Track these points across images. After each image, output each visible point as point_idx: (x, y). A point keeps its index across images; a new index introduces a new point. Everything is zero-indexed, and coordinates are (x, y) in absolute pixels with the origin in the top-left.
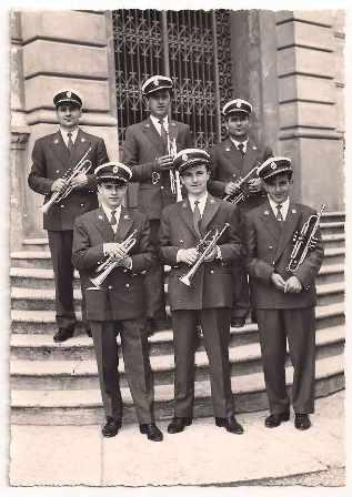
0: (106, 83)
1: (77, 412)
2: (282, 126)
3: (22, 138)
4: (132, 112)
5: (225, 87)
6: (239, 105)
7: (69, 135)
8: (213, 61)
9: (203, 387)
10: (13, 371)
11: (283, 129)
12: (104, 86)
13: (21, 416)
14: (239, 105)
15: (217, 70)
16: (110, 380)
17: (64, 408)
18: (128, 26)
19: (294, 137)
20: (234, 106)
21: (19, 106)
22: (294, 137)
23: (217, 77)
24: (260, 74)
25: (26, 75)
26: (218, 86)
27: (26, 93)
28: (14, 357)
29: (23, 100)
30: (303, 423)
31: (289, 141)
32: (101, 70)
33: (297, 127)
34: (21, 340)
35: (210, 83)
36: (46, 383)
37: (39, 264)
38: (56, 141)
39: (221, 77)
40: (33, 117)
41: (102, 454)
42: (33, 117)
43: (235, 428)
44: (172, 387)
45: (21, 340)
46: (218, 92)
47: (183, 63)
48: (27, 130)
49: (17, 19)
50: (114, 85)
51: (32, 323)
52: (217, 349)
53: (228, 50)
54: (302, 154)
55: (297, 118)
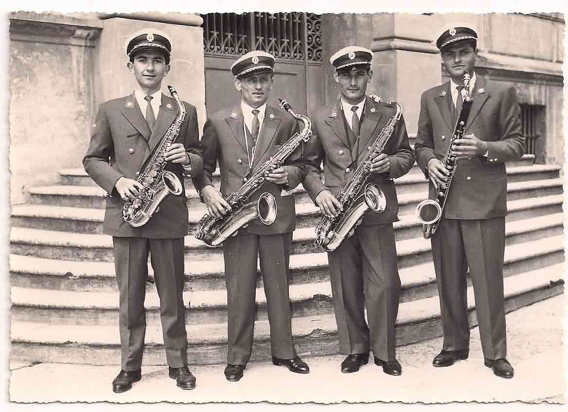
2: (375, 36)
3: (92, 32)
4: (218, 29)
5: (314, 47)
9: (262, 327)
10: (15, 336)
11: (375, 40)
13: (25, 314)
16: (135, 320)
18: (212, 44)
19: (389, 49)
22: (389, 49)
30: (392, 367)
31: (384, 53)
33: (392, 38)
37: (79, 201)
39: (309, 36)
44: (225, 293)
46: (307, 52)
48: (99, 24)
49: (102, 29)
52: (279, 317)
53: (318, 34)
54: (399, 69)
55: (393, 29)
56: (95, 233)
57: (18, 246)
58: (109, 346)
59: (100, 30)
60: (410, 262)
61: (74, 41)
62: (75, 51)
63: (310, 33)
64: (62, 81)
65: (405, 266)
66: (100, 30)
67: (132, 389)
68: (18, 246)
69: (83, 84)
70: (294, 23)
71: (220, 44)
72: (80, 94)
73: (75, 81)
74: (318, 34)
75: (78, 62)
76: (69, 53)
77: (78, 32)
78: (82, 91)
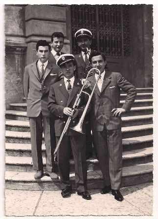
0: (65, 23)
1: (30, 184)
6: (82, 32)
7: (69, 81)
8: (120, 14)
12: (64, 25)
14: (82, 32)
15: (122, 19)
17: (25, 182)
20: (80, 33)
21: (22, 34)
23: (122, 22)
24: (143, 20)
25: (26, 19)
26: (122, 26)
27: (26, 28)
28: (7, 155)
29: (24, 31)
30: (119, 197)
32: (62, 17)
34: (12, 175)
35: (118, 25)
36: (18, 168)
38: (61, 85)
40: (28, 40)
41: (36, 207)
42: (28, 40)
43: (89, 198)
45: (12, 175)
47: (111, 16)
50: (70, 25)
51: (17, 138)
56: (11, 130)
57: (8, 139)
58: (31, 182)
59: (27, 47)
60: (140, 123)
61: (16, 53)
62: (16, 57)
63: (125, 45)
64: (11, 69)
65: (7, 70)
66: (27, 47)
67: (70, 198)
68: (8, 139)
69: (20, 69)
70: (117, 41)
71: (127, 89)
72: (19, 73)
73: (17, 68)
74: (128, 45)
75: (18, 61)
76: (14, 58)
77: (18, 49)
78: (20, 72)
